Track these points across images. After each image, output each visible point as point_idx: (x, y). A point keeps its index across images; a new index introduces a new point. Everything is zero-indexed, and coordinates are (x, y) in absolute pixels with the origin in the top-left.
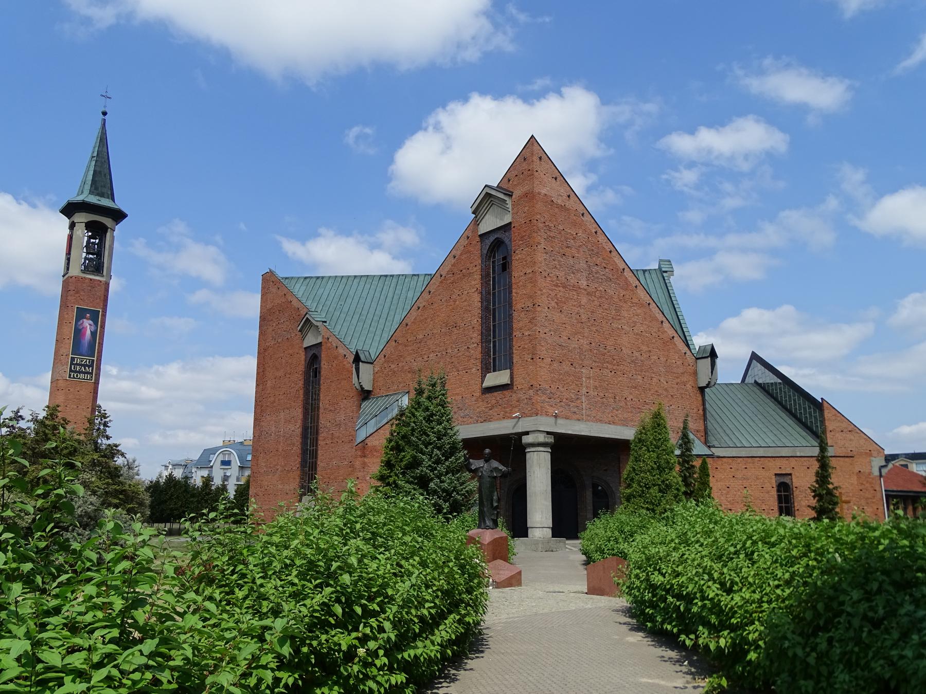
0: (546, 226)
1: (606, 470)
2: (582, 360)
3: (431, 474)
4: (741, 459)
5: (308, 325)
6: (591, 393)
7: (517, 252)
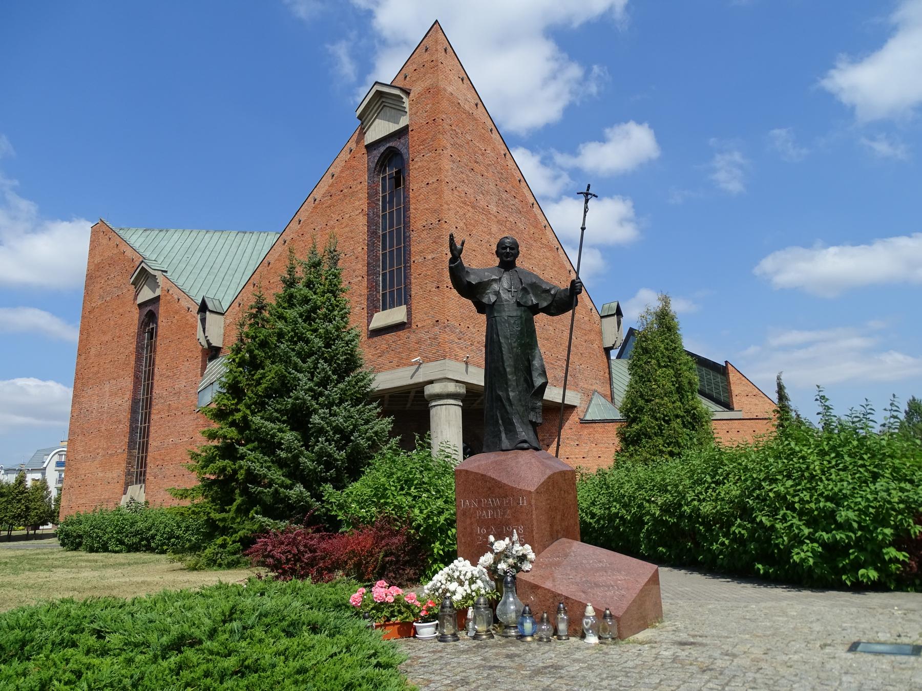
0: (452, 130)
3: (314, 403)
5: (144, 276)
7: (415, 160)
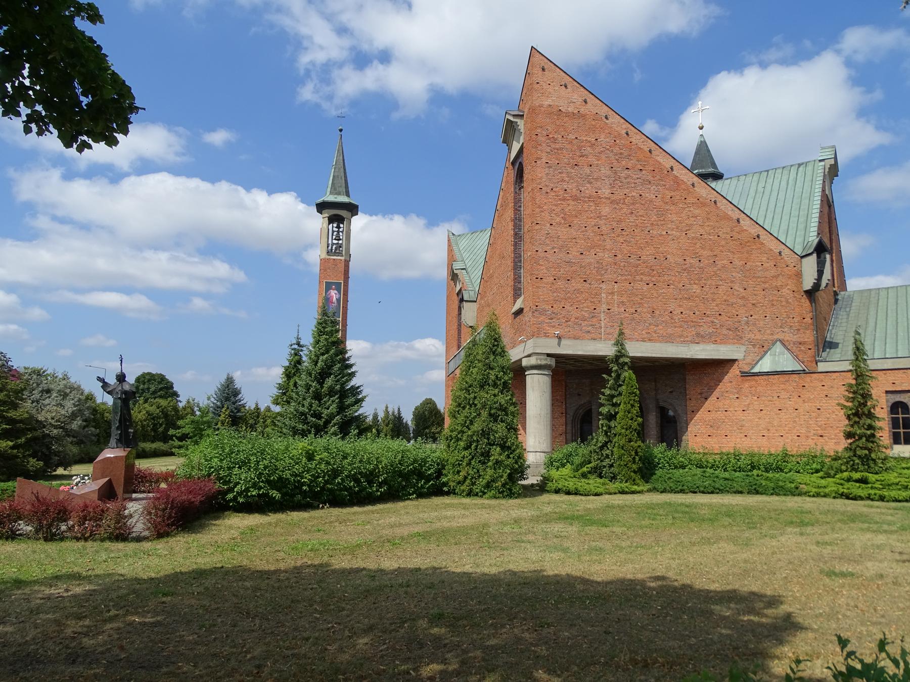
1: (671, 392)
2: (602, 275)
4: (838, 374)
6: (615, 309)
